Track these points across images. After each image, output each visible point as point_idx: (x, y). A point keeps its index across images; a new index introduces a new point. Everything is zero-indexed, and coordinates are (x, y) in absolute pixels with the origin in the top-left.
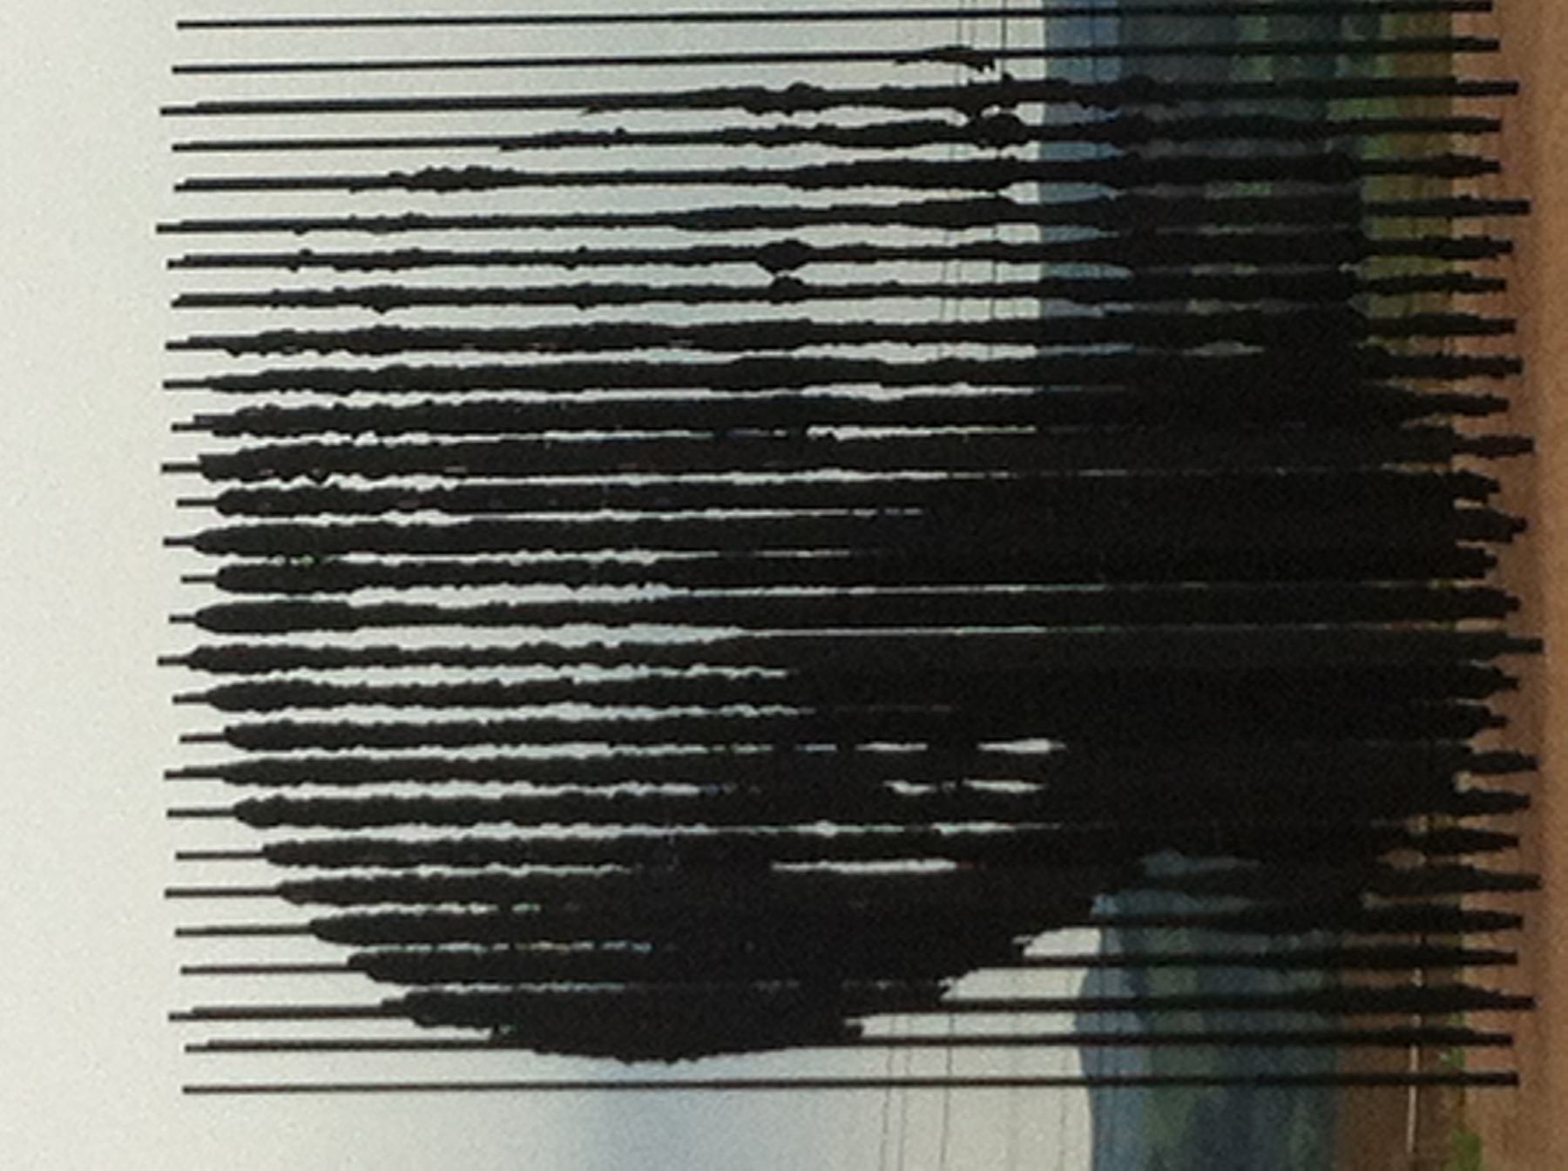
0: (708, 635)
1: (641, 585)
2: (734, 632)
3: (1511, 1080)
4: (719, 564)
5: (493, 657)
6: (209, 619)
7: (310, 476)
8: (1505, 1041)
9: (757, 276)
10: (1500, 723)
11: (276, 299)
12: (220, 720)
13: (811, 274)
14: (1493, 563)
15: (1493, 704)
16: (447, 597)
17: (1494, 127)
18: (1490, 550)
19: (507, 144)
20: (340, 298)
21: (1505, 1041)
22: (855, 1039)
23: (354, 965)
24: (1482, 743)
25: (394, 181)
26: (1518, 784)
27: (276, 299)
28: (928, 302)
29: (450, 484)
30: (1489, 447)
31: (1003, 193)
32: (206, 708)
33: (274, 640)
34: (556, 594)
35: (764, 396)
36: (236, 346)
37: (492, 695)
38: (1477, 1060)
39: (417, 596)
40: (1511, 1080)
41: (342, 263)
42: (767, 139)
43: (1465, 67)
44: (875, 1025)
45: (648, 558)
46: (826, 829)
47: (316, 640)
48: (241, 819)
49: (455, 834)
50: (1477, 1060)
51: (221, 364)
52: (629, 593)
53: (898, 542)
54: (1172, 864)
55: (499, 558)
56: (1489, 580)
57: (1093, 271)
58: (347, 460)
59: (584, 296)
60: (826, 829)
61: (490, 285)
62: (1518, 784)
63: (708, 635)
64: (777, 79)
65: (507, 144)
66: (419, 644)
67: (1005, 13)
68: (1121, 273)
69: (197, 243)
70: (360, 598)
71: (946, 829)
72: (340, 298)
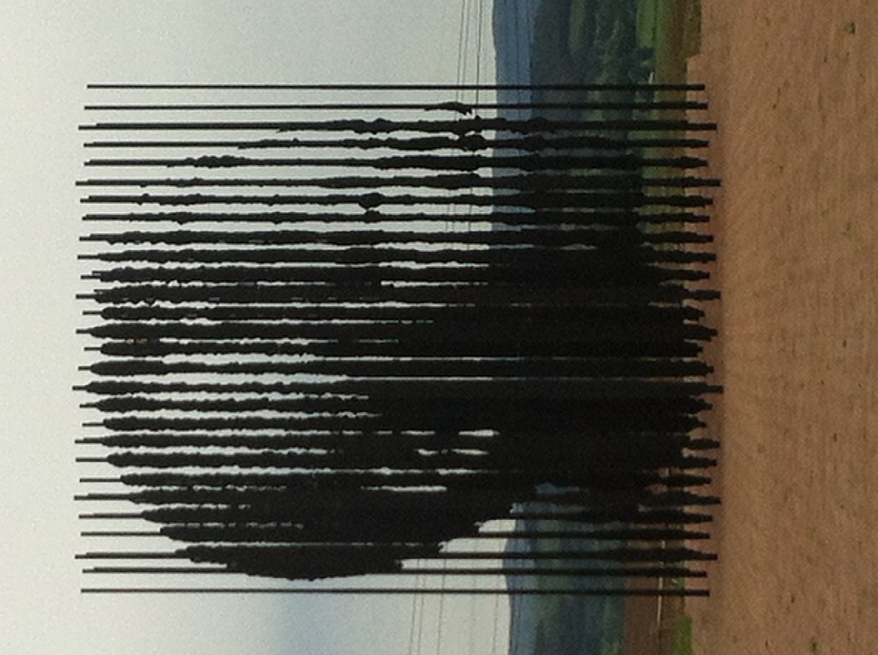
0: (332, 379)
1: (301, 355)
2: (344, 378)
3: (706, 593)
4: (340, 342)
5: (230, 388)
6: (97, 369)
7: (146, 302)
8: (703, 574)
9: (357, 210)
10: (704, 425)
11: (132, 218)
12: (101, 416)
14: (701, 350)
16: (210, 359)
17: (705, 144)
18: (699, 343)
21: (703, 574)
22: (399, 570)
23: (163, 532)
24: (695, 434)
26: (711, 454)
27: (132, 218)
28: (438, 222)
29: (212, 306)
30: (699, 296)
31: (475, 172)
33: (128, 379)
34: (262, 358)
35: (361, 266)
36: (113, 239)
37: (231, 406)
38: (690, 584)
39: (196, 359)
40: (706, 593)
41: (162, 201)
43: (692, 117)
44: (408, 564)
45: (305, 342)
46: (386, 471)
47: (147, 379)
48: (110, 463)
49: (212, 471)
50: (690, 584)
51: (104, 247)
52: (295, 359)
53: (406, 335)
54: (551, 489)
55: (235, 341)
56: (700, 358)
58: (163, 293)
59: (277, 218)
60: (386, 471)
61: (232, 215)
62: (711, 454)
63: (332, 379)
64: (369, 116)
65: (242, 145)
66: (197, 379)
70: (170, 359)
71: (443, 472)
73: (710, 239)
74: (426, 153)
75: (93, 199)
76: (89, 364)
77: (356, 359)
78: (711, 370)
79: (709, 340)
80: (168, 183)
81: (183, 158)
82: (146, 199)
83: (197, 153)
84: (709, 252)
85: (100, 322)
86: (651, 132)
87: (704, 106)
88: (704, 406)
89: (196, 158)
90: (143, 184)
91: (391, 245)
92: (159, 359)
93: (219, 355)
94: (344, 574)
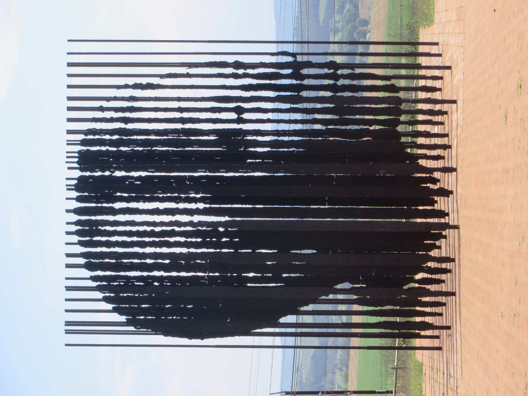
3: (440, 349)
6: (78, 211)
7: (110, 171)
9: (233, 116)
13: (246, 116)
14: (436, 202)
15: (437, 243)
16: (141, 205)
17: (441, 78)
19: (162, 76)
20: (112, 120)
23: (114, 310)
24: (434, 253)
25: (126, 86)
28: (270, 122)
32: (72, 214)
35: (233, 146)
40: (440, 349)
41: (116, 110)
42: (236, 76)
46: (251, 275)
47: (111, 218)
52: (193, 206)
54: (347, 285)
57: (328, 117)
59: (183, 121)
60: (251, 275)
61: (155, 119)
65: (162, 76)
67: (308, 42)
68: (335, 117)
69: (75, 105)
70: (118, 205)
72: (112, 120)
73: (446, 135)
74: (273, 82)
75: (433, 89)
76: (72, 208)
77: (229, 206)
78: (447, 215)
79: (448, 197)
80: (123, 99)
81: (123, 84)
82: (102, 109)
83: (131, 81)
84: (447, 143)
85: (74, 228)
86: (346, 80)
87: (440, 55)
88: (440, 236)
89: (131, 83)
90: (179, 99)
91: (255, 138)
92: (111, 205)
93: (147, 203)
94: (222, 336)
